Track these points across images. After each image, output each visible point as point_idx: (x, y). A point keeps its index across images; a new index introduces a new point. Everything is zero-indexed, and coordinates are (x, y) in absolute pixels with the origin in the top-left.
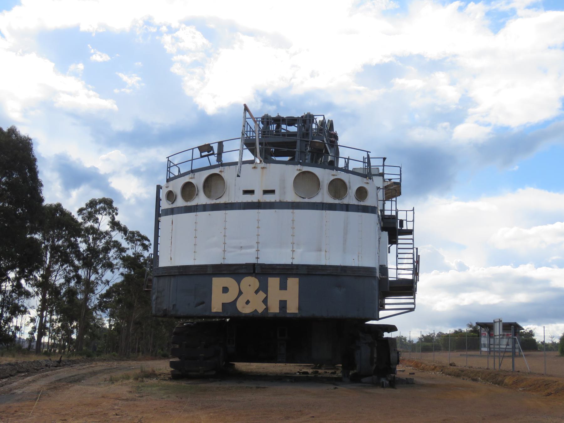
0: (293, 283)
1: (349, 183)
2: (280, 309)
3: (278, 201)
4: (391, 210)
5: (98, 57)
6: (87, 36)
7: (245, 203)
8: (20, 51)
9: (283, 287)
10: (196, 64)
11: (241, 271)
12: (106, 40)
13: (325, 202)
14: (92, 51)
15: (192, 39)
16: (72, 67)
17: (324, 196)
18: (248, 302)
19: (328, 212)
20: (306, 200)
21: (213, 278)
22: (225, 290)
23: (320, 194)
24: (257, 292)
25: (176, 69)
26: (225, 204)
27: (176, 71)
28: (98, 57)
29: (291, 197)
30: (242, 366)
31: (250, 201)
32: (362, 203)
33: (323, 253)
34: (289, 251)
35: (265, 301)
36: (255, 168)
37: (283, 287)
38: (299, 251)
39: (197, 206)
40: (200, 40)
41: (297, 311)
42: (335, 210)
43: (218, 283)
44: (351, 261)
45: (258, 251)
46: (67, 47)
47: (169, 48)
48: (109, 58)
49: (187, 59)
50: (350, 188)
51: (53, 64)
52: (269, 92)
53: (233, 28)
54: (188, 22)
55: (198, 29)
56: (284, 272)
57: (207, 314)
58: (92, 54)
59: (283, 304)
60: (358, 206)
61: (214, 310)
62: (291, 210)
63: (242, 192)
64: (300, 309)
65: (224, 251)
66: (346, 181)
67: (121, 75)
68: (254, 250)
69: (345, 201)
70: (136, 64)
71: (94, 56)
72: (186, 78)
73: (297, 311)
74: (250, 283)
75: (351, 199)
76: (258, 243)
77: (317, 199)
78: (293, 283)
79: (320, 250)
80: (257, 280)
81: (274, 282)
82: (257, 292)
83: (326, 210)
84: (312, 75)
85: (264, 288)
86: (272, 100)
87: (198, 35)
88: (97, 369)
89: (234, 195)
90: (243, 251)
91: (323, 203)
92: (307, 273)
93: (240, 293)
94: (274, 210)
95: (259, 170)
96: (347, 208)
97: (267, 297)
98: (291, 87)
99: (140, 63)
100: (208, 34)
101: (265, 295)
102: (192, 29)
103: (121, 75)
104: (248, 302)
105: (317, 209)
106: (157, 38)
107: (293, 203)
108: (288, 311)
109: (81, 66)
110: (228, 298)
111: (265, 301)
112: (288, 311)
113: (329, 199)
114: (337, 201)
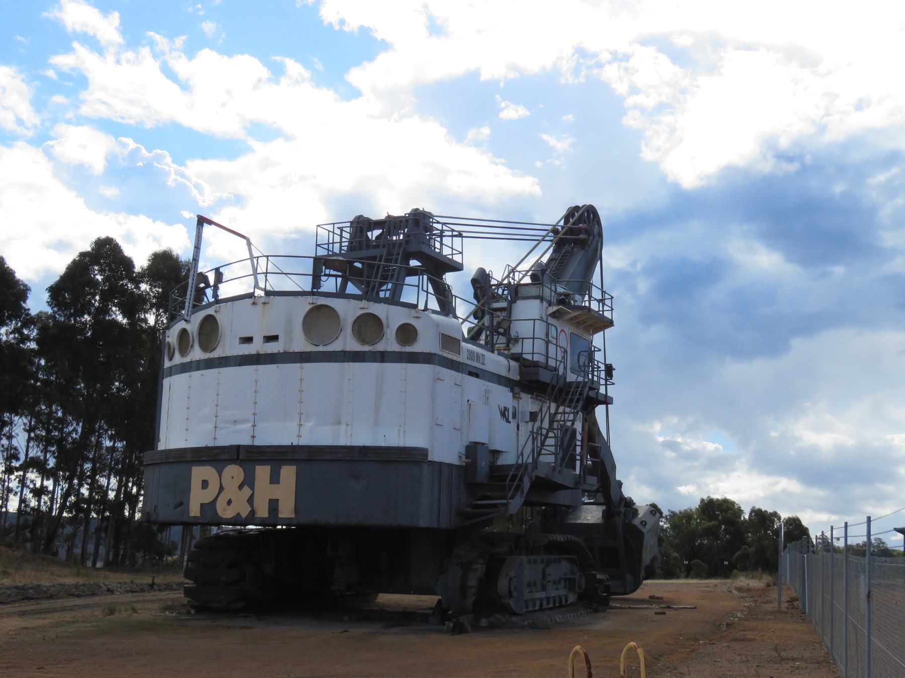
0: (289, 473)
1: (387, 318)
2: (270, 513)
3: (282, 351)
4: (533, 353)
5: (511, 112)
6: (492, 85)
7: (236, 356)
8: (396, 116)
9: (275, 479)
10: (662, 108)
11: (222, 457)
12: (522, 88)
13: (348, 349)
14: (503, 105)
15: (653, 72)
16: (471, 134)
17: (348, 342)
18: (229, 502)
19: (352, 364)
20: (321, 348)
21: (193, 468)
22: (205, 484)
23: (340, 339)
24: (241, 487)
25: (631, 121)
26: (220, 358)
27: (632, 123)
28: (511, 112)
29: (300, 344)
30: (385, 599)
31: (247, 353)
32: (408, 349)
33: (343, 427)
34: (295, 425)
35: (251, 500)
36: (254, 304)
37: (275, 479)
38: (308, 425)
39: (191, 362)
40: (667, 68)
41: (293, 516)
42: (363, 361)
43: (199, 473)
44: (389, 437)
45: (254, 426)
46: (462, 103)
47: (621, 88)
48: (528, 113)
49: (650, 102)
50: (388, 326)
51: (445, 131)
52: (784, 143)
53: (717, 43)
54: (644, 42)
55: (660, 50)
56: (276, 456)
57: (185, 519)
58: (502, 110)
59: (274, 505)
60: (401, 353)
61: (192, 514)
62: (299, 365)
63: (238, 341)
64: (296, 510)
65: (216, 427)
66: (382, 316)
67: (545, 137)
68: (248, 426)
69: (380, 347)
70: (565, 118)
71: (505, 111)
72: (648, 133)
73: (293, 516)
74: (234, 473)
75: (389, 343)
76: (255, 414)
77: (336, 346)
78: (289, 473)
79: (339, 423)
80: (241, 470)
81: (263, 472)
82: (241, 487)
83: (348, 361)
84: (859, 106)
85: (249, 481)
86: (792, 154)
87: (664, 59)
88: (147, 598)
89: (229, 347)
90: (238, 427)
91: (345, 352)
92: (306, 457)
93: (221, 489)
94: (275, 365)
95: (260, 306)
96: (383, 357)
97: (252, 495)
98: (822, 129)
99: (570, 116)
100: (678, 56)
101: (250, 492)
102: (651, 50)
103: (545, 137)
104: (229, 502)
105: (336, 361)
106: (595, 71)
107: (302, 353)
108: (280, 516)
109: (486, 131)
110: (207, 496)
111: (251, 500)
112: (280, 516)
113: (354, 345)
114: (366, 348)
